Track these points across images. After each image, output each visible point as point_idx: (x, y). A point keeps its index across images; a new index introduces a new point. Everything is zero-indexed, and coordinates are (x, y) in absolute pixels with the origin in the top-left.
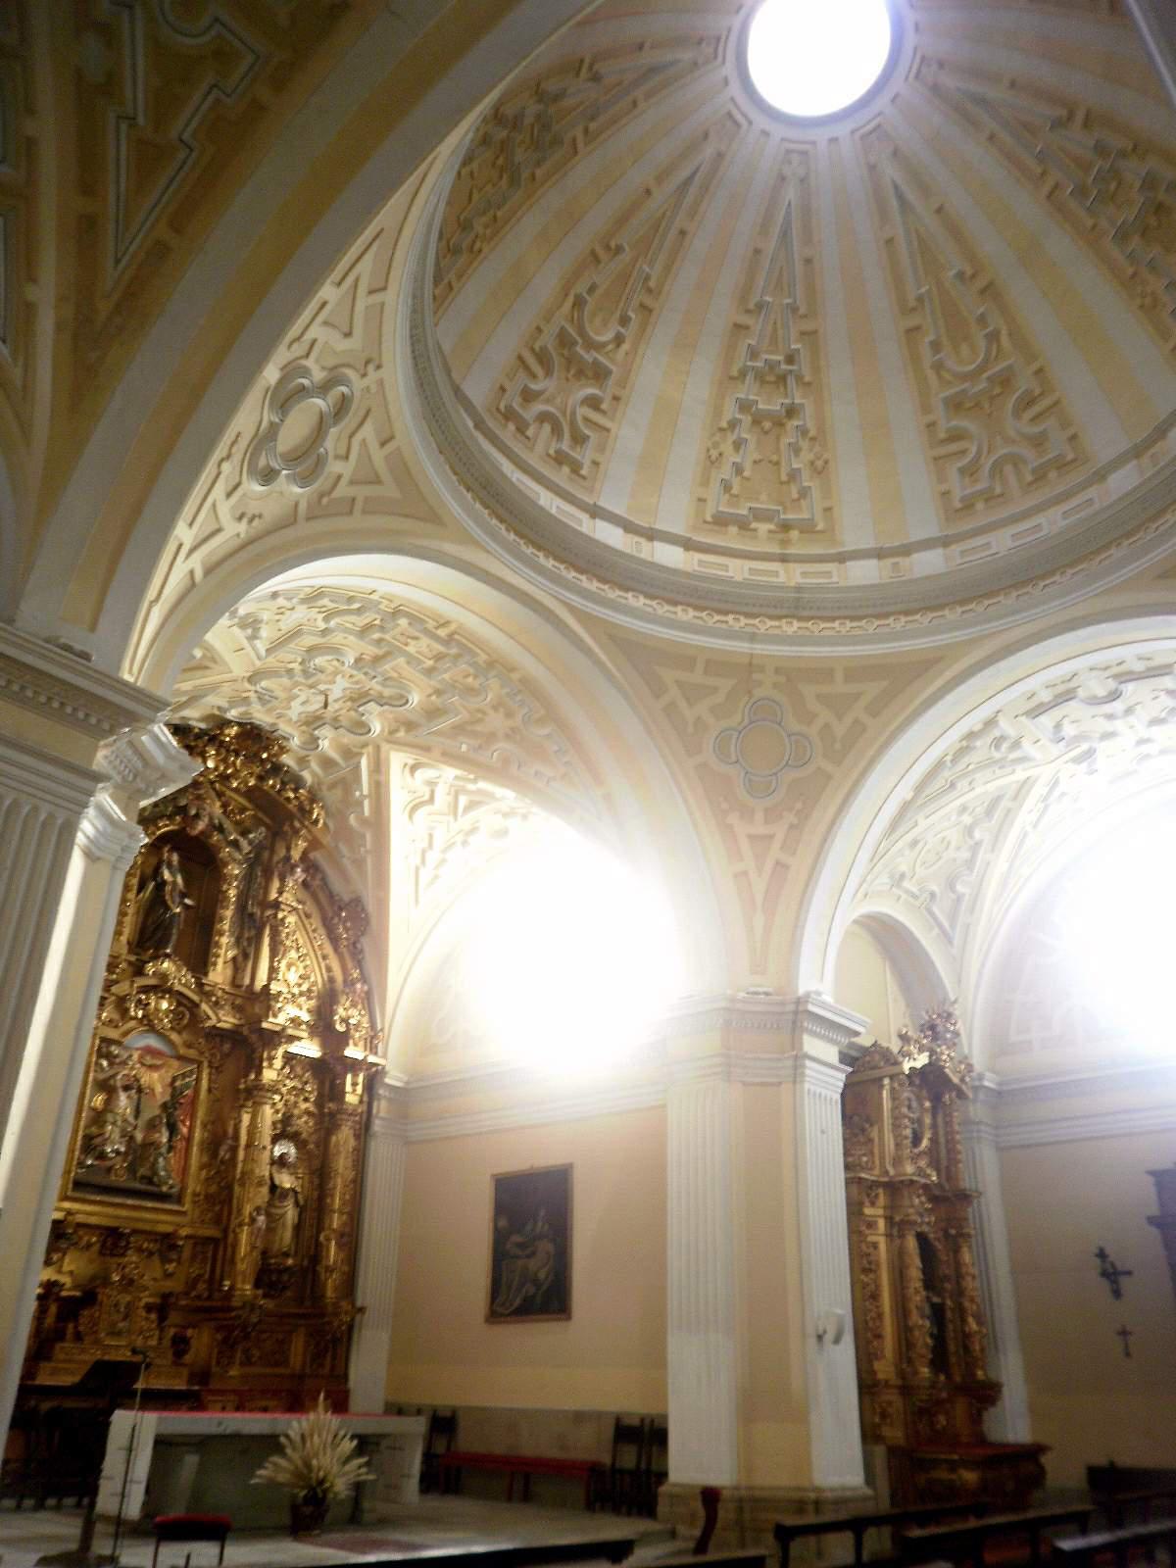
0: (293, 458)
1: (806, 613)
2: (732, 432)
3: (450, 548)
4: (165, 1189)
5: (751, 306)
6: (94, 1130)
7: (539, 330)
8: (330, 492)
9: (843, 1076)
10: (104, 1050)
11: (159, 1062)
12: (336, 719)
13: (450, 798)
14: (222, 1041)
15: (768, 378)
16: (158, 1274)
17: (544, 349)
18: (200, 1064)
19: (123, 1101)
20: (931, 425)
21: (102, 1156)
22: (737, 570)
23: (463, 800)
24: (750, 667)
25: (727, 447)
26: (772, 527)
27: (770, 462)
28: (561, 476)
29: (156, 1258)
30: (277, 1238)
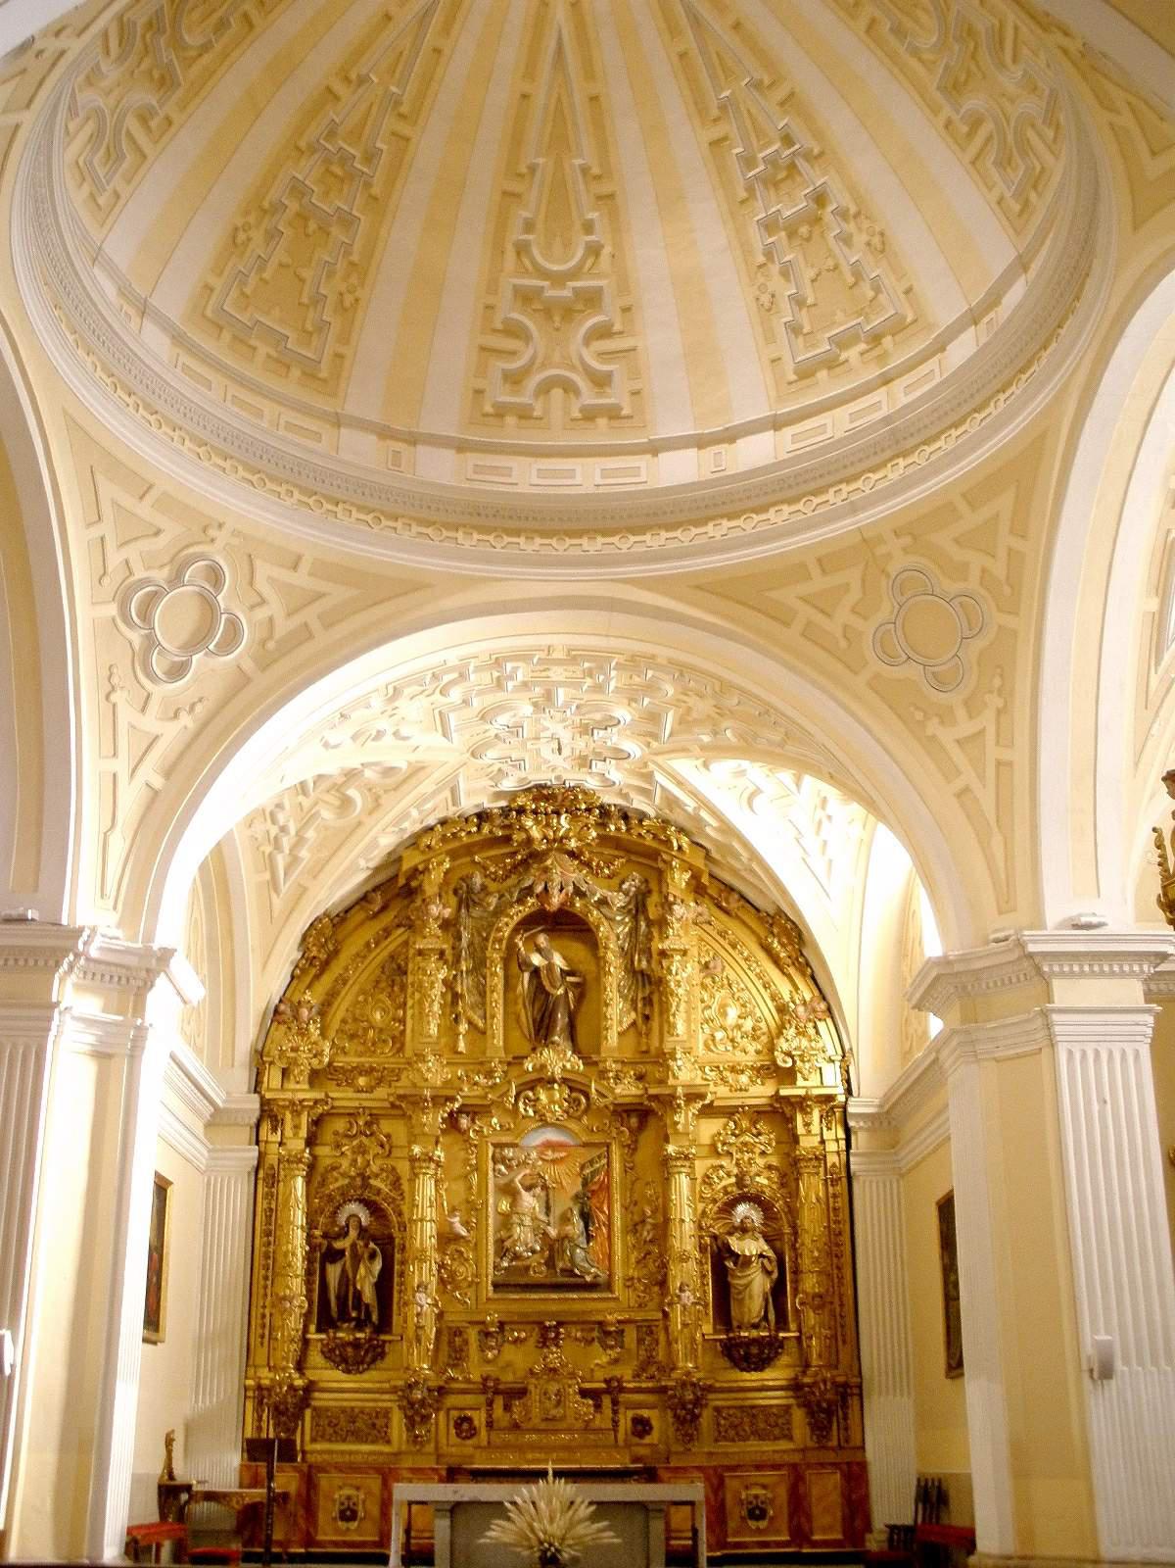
0: (196, 642)
1: (912, 442)
2: (773, 262)
3: (449, 603)
4: (588, 1279)
5: (715, 112)
7: (489, 307)
8: (271, 636)
9: (1150, 1019)
10: (497, 1155)
11: (563, 1154)
14: (628, 1116)
15: (780, 177)
17: (506, 321)
18: (608, 1146)
19: (529, 1201)
20: (948, 124)
21: (517, 1257)
22: (837, 424)
24: (866, 543)
25: (776, 283)
26: (863, 346)
27: (828, 270)
28: (601, 433)
29: (596, 1344)
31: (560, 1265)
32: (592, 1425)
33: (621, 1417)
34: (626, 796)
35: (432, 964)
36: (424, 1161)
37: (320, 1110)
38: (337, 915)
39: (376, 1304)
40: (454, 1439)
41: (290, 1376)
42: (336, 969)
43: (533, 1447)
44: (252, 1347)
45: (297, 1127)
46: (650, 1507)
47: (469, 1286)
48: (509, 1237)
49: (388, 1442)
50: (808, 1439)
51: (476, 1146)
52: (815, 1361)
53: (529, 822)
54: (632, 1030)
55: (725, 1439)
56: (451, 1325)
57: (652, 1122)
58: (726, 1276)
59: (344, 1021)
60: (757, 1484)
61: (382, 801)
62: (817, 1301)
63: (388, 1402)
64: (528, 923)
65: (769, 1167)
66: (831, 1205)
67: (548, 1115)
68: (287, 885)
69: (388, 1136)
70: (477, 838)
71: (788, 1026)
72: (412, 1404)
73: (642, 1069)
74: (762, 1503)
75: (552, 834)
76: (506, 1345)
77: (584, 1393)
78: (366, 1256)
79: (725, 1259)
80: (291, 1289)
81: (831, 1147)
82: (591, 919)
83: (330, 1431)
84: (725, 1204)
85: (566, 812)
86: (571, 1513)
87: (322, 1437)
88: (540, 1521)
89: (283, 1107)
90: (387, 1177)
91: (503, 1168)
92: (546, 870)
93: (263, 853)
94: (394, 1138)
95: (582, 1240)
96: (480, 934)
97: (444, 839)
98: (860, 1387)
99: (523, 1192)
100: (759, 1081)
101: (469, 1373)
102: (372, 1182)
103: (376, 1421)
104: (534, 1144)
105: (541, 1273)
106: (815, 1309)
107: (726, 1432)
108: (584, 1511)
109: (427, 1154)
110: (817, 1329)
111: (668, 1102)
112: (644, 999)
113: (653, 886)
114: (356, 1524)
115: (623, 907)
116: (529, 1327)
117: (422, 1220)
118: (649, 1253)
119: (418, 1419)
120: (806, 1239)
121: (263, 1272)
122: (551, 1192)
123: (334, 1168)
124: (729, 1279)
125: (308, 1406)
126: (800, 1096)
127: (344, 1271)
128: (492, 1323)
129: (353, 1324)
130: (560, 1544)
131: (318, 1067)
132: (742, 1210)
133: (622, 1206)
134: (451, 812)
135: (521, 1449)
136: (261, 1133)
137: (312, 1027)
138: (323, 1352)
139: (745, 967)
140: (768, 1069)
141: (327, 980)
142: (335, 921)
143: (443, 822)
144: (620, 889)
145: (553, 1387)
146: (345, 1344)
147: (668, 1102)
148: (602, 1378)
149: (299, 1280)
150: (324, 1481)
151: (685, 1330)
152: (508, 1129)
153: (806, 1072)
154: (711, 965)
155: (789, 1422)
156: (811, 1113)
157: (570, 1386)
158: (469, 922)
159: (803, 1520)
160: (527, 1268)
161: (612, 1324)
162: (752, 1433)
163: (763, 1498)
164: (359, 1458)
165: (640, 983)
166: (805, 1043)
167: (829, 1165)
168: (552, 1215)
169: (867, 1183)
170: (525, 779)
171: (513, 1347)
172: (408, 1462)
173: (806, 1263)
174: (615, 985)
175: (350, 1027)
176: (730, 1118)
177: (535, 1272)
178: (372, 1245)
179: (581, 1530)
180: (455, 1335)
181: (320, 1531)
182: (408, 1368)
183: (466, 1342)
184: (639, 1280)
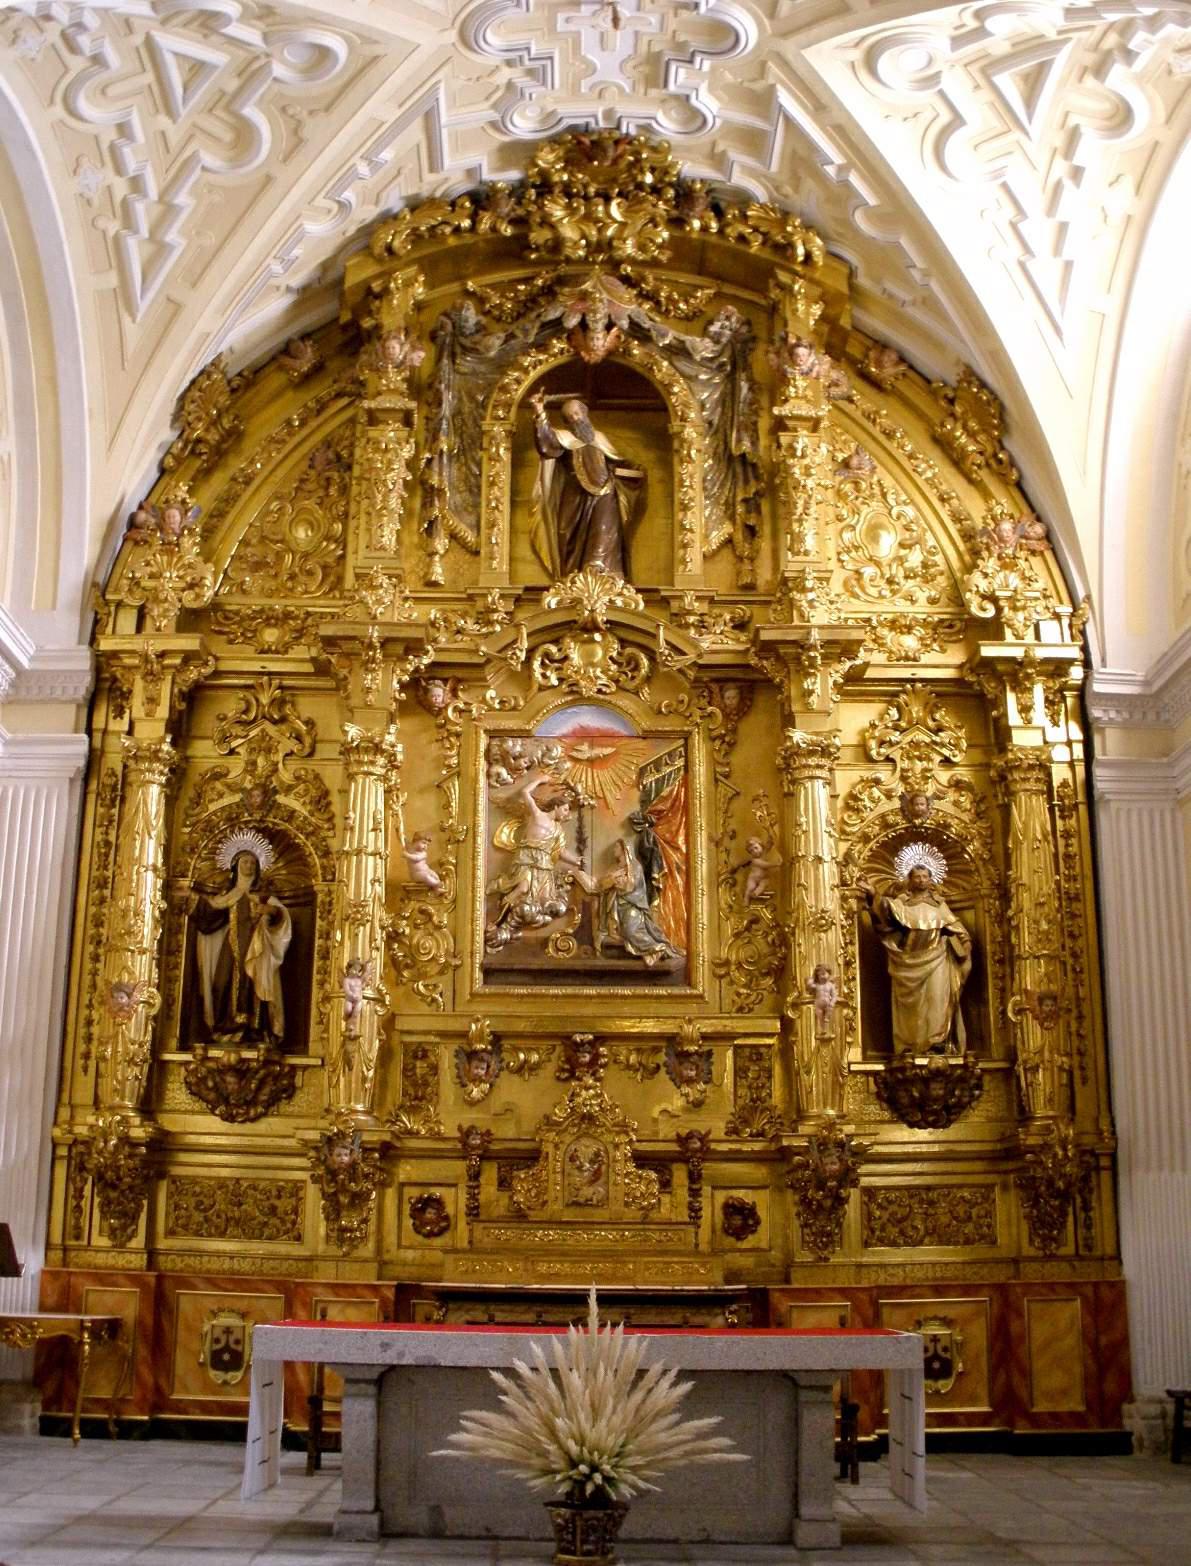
4: (650, 961)
6: (503, 883)
10: (495, 750)
11: (608, 751)
12: (680, 47)
13: (986, 95)
16: (678, 1103)
18: (687, 737)
19: (548, 828)
21: (525, 923)
23: (1008, 83)
29: (663, 1074)
30: (920, 1022)
31: (601, 938)
32: (654, 1215)
33: (705, 1202)
34: (719, 160)
35: (391, 432)
36: (366, 750)
37: (193, 674)
38: (240, 374)
39: (280, 1004)
40: (410, 1236)
41: (125, 1120)
42: (236, 464)
43: (548, 1252)
44: (68, 1073)
45: (152, 701)
46: (803, 1381)
47: (441, 973)
48: (514, 888)
49: (299, 1238)
50: (1025, 1242)
51: (458, 735)
52: (1040, 1110)
53: (557, 210)
54: (726, 553)
55: (882, 1242)
56: (408, 1039)
57: (761, 701)
58: (885, 967)
59: (245, 543)
60: (935, 1318)
61: (306, 133)
62: (1048, 1005)
63: (298, 1171)
64: (554, 381)
65: (957, 785)
66: (1061, 850)
67: (583, 683)
68: (151, 295)
69: (310, 723)
70: (468, 239)
71: (985, 554)
72: (333, 1173)
73: (741, 611)
74: (945, 1349)
75: (594, 232)
76: (504, 1074)
77: (641, 1160)
78: (265, 919)
79: (884, 935)
80: (131, 973)
81: (1060, 754)
82: (659, 376)
83: (198, 1217)
84: (884, 845)
85: (620, 195)
86: (638, 1396)
87: (185, 1227)
88: (570, 1415)
89: (130, 668)
90: (307, 791)
91: (504, 772)
92: (584, 296)
93: (104, 233)
94: (320, 724)
95: (640, 895)
96: (472, 398)
97: (416, 237)
98: (1113, 1157)
99: (539, 813)
100: (935, 646)
101: (438, 1122)
102: (281, 799)
103: (277, 1203)
104: (558, 733)
105: (568, 950)
106: (1042, 1020)
107: (883, 1229)
108: (667, 1393)
109: (371, 740)
110: (1047, 1054)
111: (792, 656)
112: (745, 501)
113: (761, 331)
114: (239, 1375)
115: (711, 360)
116: (545, 1044)
117: (359, 852)
118: (755, 920)
119: (344, 1200)
120: (1025, 900)
121: (90, 948)
122: (586, 813)
123: (217, 776)
124: (891, 969)
125: (162, 1175)
126: (1012, 660)
127: (226, 946)
128: (480, 1038)
129: (239, 1036)
130: (615, 1467)
131: (195, 605)
132: (913, 856)
133: (710, 839)
134: (429, 184)
135: (529, 1255)
136: (95, 718)
137: (187, 542)
138: (188, 1084)
139: (909, 469)
140: (951, 626)
141: (218, 482)
142: (234, 384)
143: (415, 205)
144: (704, 333)
145: (587, 1149)
146: (224, 1070)
147: (792, 656)
148: (672, 1135)
149: (146, 958)
150: (187, 1303)
151: (824, 1051)
152: (514, 709)
153: (1019, 625)
154: (854, 462)
155: (989, 1214)
156: (1030, 690)
157: (617, 1146)
158: (456, 380)
159: (1016, 1379)
160: (544, 943)
161: (692, 1041)
162: (927, 1233)
163: (944, 1342)
164: (246, 1266)
165: (741, 477)
166: (1014, 580)
167: (1056, 783)
168: (587, 852)
169: (1123, 815)
170: (553, 113)
171: (516, 1078)
172: (327, 1273)
173: (1026, 941)
174: (697, 479)
175: (253, 553)
176: (890, 703)
177: (558, 950)
178: (273, 901)
179: (660, 1433)
180: (416, 1057)
181: (177, 1385)
182: (328, 1111)
183: (434, 1069)
184: (739, 966)
